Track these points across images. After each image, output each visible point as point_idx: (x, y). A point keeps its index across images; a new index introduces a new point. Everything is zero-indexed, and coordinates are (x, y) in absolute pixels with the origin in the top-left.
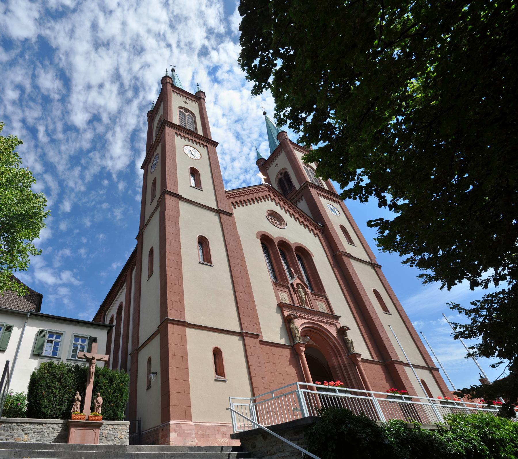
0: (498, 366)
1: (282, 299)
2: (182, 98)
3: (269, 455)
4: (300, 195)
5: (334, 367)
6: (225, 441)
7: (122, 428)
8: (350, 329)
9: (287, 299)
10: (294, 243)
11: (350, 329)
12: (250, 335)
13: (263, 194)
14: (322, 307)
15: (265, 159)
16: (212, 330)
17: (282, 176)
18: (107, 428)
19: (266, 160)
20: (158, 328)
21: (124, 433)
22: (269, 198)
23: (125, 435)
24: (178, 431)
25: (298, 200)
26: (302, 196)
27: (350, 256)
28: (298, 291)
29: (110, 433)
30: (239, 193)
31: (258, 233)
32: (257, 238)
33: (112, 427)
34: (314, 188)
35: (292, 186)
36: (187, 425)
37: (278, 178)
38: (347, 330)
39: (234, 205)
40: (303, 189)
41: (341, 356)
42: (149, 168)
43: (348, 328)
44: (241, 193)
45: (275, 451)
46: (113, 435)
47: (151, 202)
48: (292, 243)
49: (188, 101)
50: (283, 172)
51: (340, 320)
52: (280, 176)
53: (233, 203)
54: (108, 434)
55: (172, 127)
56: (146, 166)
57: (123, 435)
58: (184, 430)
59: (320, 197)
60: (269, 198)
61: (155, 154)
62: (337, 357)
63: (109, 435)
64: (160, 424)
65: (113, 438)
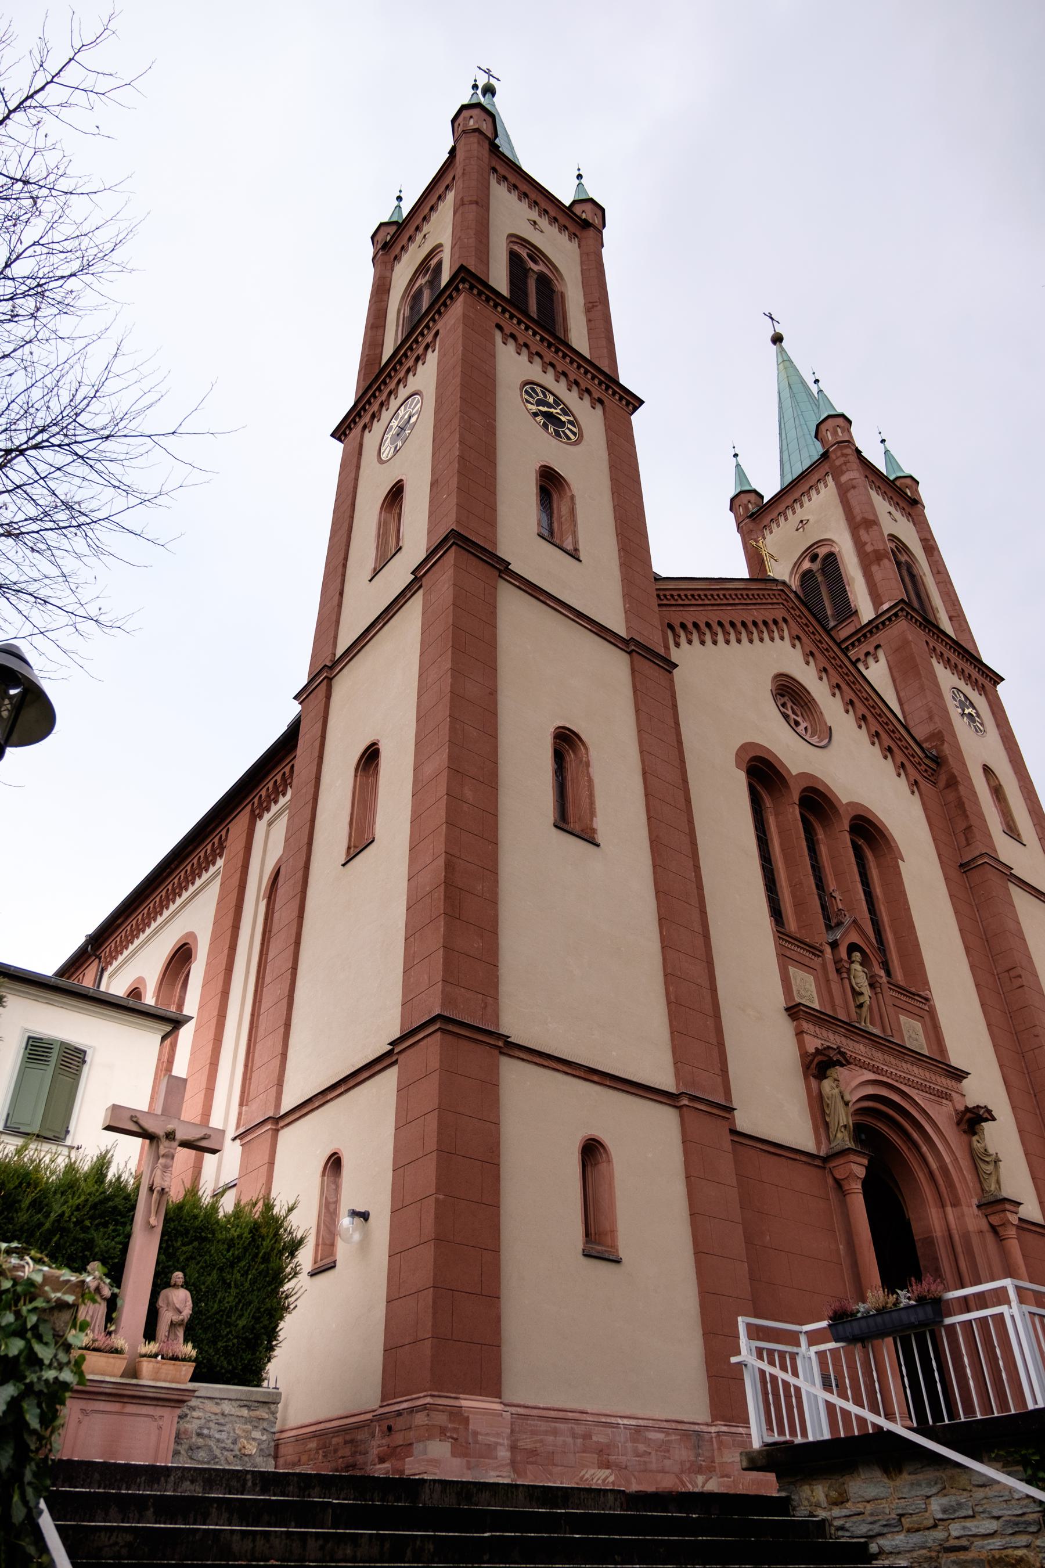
0: (296, 1306)
1: (799, 991)
2: (524, 205)
3: (909, 1531)
4: (874, 640)
5: (930, 1241)
6: (604, 1480)
7: (253, 1414)
8: (994, 1119)
9: (815, 995)
10: (849, 804)
11: (994, 1119)
12: (702, 1107)
13: (769, 615)
14: (914, 1036)
15: (762, 497)
16: (582, 1074)
17: (816, 566)
18: (195, 1414)
19: (765, 501)
20: (390, 1047)
21: (256, 1434)
22: (786, 634)
23: (260, 1442)
24: (455, 1436)
25: (862, 657)
26: (878, 647)
27: (1008, 875)
28: (849, 970)
29: (205, 1431)
30: (693, 596)
31: (745, 747)
32: (738, 766)
33: (217, 1409)
34: (920, 627)
35: (846, 611)
36: (484, 1414)
37: (801, 571)
38: (986, 1120)
39: (676, 636)
40: (883, 623)
41: (956, 1204)
42: (371, 440)
43: (989, 1112)
44: (699, 596)
45: (940, 1516)
46: (218, 1440)
47: (376, 573)
48: (844, 802)
49: (543, 222)
50: (822, 551)
51: (965, 1081)
52: (806, 565)
53: (670, 626)
54: (199, 1435)
55: (488, 300)
56: (356, 431)
57: (255, 1444)
58: (475, 1434)
59: (934, 661)
60: (786, 634)
61: (403, 393)
62: (943, 1206)
63: (200, 1441)
64: (379, 1403)
65: (217, 1452)
